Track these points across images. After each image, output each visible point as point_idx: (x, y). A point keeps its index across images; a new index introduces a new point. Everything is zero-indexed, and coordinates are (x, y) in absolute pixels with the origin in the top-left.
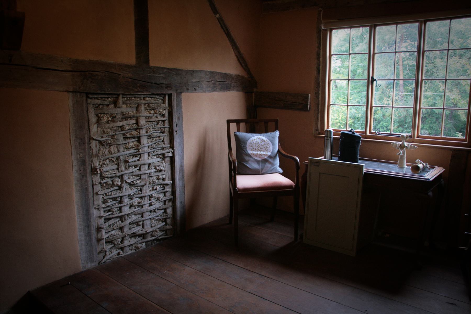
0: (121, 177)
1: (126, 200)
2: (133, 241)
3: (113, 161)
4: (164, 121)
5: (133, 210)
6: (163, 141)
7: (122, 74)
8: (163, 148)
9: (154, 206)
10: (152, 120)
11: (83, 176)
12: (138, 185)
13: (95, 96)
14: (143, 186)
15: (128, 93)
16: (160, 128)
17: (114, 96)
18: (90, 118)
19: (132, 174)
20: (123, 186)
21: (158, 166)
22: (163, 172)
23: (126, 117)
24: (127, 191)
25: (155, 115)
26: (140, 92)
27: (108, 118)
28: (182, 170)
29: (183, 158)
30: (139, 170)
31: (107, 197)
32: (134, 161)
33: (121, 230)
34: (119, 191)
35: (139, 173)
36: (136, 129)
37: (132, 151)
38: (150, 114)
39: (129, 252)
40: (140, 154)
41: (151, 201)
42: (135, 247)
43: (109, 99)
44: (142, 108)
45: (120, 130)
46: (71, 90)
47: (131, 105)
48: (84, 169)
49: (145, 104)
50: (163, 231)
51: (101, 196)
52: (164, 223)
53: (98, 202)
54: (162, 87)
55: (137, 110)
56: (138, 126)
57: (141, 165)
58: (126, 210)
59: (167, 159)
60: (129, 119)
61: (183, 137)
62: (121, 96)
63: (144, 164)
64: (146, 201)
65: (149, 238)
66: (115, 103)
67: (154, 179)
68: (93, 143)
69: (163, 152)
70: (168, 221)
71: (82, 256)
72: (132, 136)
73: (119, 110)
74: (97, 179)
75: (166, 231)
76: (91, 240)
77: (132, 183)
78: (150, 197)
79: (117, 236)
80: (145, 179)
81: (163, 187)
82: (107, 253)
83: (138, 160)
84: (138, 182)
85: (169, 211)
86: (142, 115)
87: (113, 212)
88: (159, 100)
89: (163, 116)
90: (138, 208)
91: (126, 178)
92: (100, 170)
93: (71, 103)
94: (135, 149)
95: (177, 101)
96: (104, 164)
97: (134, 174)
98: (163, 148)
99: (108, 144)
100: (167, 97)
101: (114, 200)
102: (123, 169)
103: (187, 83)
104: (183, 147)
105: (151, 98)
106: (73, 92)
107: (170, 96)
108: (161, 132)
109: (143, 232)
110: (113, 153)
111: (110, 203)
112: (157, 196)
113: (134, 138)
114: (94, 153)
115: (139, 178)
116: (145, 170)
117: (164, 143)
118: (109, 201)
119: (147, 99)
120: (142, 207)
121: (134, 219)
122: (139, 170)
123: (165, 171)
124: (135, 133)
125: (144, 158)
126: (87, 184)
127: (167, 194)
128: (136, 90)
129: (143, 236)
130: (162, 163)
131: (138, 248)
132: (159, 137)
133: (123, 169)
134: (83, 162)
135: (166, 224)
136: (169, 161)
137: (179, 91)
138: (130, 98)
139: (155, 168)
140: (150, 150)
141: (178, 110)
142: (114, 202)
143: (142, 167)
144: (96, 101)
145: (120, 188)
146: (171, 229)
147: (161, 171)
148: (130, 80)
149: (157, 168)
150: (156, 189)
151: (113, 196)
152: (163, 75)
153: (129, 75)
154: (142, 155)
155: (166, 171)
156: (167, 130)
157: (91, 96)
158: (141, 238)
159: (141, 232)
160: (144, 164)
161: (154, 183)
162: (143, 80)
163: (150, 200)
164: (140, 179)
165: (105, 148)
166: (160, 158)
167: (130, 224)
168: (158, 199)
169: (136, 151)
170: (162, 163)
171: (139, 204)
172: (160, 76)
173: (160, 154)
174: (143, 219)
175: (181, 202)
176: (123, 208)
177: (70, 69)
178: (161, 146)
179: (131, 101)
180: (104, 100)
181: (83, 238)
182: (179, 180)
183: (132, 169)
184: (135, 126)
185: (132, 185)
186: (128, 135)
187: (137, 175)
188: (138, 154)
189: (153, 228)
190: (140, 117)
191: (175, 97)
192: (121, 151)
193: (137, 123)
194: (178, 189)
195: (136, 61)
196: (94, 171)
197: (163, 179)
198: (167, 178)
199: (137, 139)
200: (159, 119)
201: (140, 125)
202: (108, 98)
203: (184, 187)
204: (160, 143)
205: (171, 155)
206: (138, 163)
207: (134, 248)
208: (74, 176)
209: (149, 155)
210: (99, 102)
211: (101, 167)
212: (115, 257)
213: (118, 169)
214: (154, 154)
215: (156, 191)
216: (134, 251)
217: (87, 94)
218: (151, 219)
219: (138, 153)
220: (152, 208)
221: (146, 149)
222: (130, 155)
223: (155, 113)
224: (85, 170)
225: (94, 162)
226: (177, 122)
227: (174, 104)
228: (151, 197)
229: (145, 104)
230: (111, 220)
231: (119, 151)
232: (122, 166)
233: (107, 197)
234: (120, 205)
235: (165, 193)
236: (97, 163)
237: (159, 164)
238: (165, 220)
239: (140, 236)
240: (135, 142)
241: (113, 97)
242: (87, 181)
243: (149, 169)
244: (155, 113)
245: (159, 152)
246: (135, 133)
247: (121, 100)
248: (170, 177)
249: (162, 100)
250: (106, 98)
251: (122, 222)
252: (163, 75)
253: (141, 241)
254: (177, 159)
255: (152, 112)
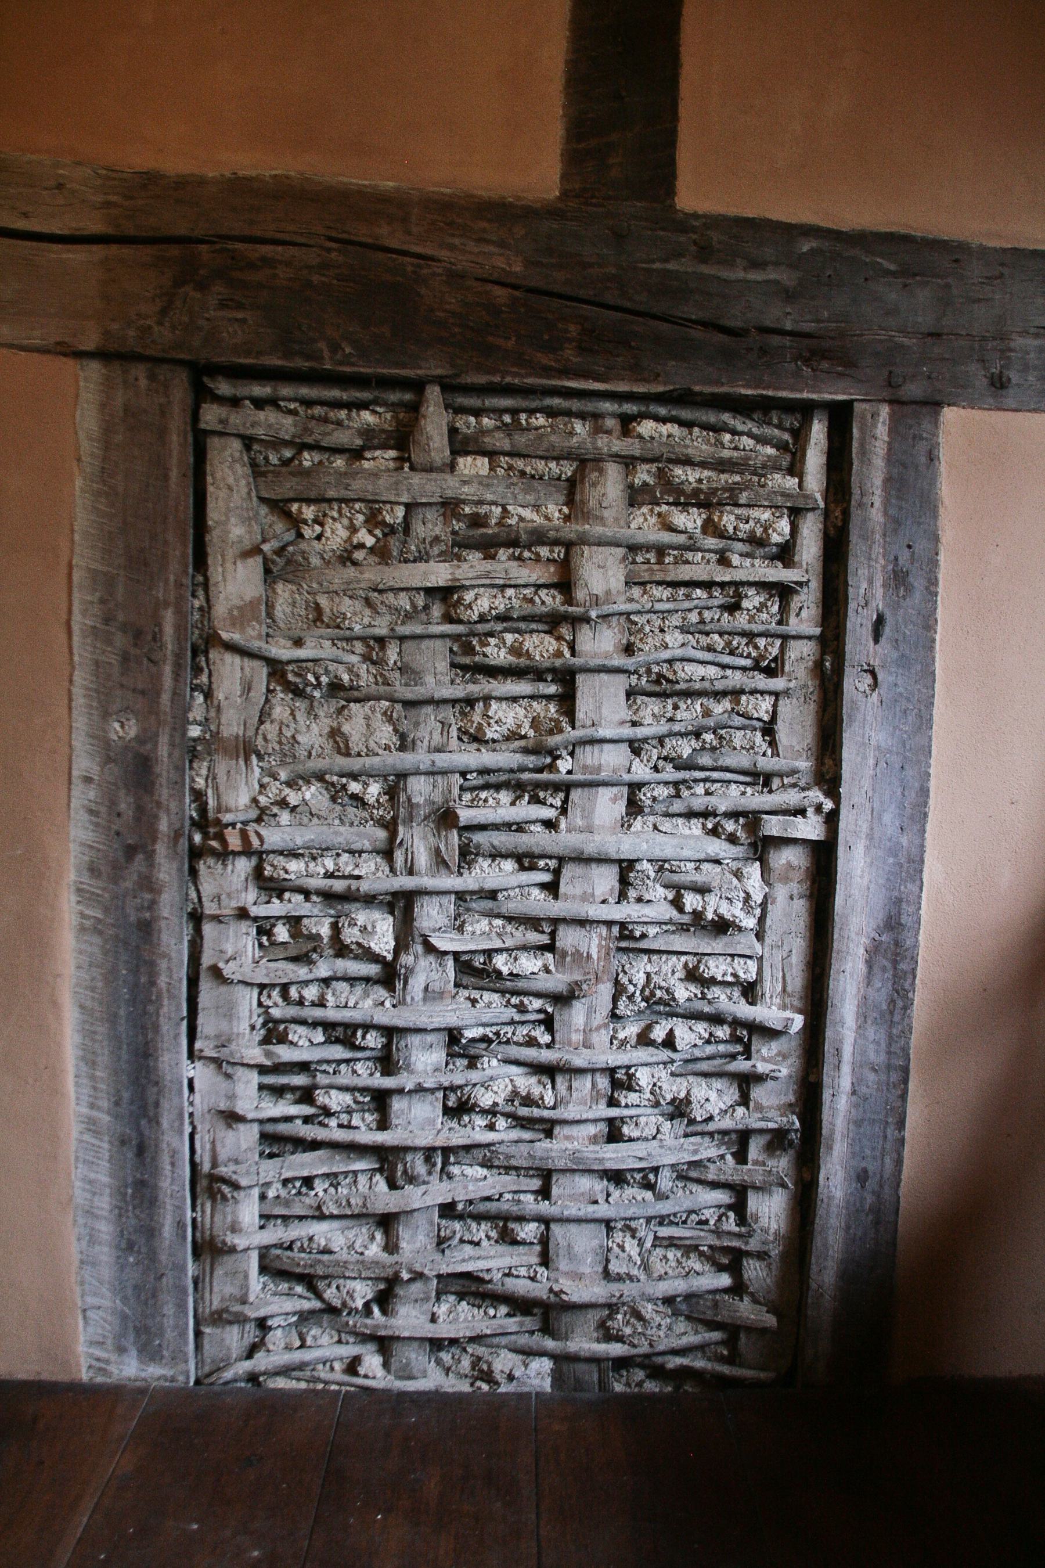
0: (402, 905)
1: (425, 1060)
2: (461, 1318)
3: (358, 800)
4: (784, 592)
5: (474, 1131)
6: (769, 730)
7: (443, 254)
8: (763, 779)
9: (639, 1149)
10: (685, 573)
11: (131, 851)
12: (521, 984)
13: (259, 390)
14: (564, 999)
15: (481, 379)
16: (750, 636)
17: (394, 397)
18: (214, 514)
19: (488, 904)
20: (410, 971)
21: (703, 890)
22: (746, 943)
23: (484, 538)
24: (434, 998)
25: (711, 542)
26: (585, 375)
27: (353, 529)
28: (893, 949)
29: (910, 867)
30: (552, 888)
31: (292, 1011)
32: (519, 827)
33: (387, 1233)
34: (381, 992)
35: (539, 903)
36: (553, 622)
37: (505, 758)
38: (672, 529)
39: (431, 1378)
40: (565, 788)
41: (614, 1112)
42: (477, 1361)
43: (367, 416)
44: (610, 487)
45: (437, 611)
46: (89, 346)
47: (520, 463)
48: (140, 809)
49: (629, 463)
50: (712, 1325)
51: (248, 998)
52: (725, 1280)
53: (224, 1026)
54: (763, 351)
55: (570, 502)
56: (569, 600)
57: (561, 860)
58: (418, 1122)
59: (789, 859)
60: (503, 554)
61: (925, 722)
62: (433, 393)
63: (584, 859)
64: (582, 1102)
65: (583, 1342)
66: (402, 440)
67: (669, 973)
68: (229, 674)
69: (755, 799)
70: (754, 1271)
71: (91, 1300)
72: (523, 661)
73: (425, 487)
74: (229, 882)
75: (733, 1331)
76: (151, 1232)
77: (479, 961)
78: (616, 1084)
79: (343, 1255)
80: (581, 958)
81: (735, 1039)
82: (276, 1338)
83: (550, 825)
84: (529, 964)
85: (770, 1210)
86: (598, 530)
87: (327, 1112)
88: (747, 440)
89: (785, 554)
90: (515, 1134)
91: (431, 916)
92: (244, 835)
93: (88, 420)
94: (526, 751)
95: (890, 458)
96: (283, 803)
97: (512, 907)
98: (763, 779)
99: (336, 688)
100: (818, 431)
101: (338, 1041)
102: (423, 859)
103: (1003, 337)
104: (924, 792)
105: (682, 423)
106: (102, 355)
107: (840, 418)
108: (756, 667)
109: (539, 1290)
110: (356, 743)
111: (304, 1045)
112: (673, 1088)
113: (538, 674)
114: (232, 725)
115: (545, 939)
116: (587, 898)
117: (773, 744)
118: (298, 1034)
119: (647, 428)
120: (549, 1134)
121: (475, 1191)
122: (552, 888)
123: (760, 936)
124: (541, 647)
125: (588, 814)
126: (153, 904)
127: (758, 1093)
128: (546, 360)
129: (548, 1313)
130: (738, 874)
131: (487, 1376)
132: (736, 693)
133: (423, 859)
134: (136, 771)
135: (738, 1289)
136: (797, 876)
137: (913, 390)
138: (514, 412)
139: (677, 903)
140: (641, 771)
141: (894, 524)
142: (338, 1052)
143: (569, 872)
144: (268, 416)
145: (390, 976)
146: (763, 1331)
147: (722, 927)
148: (500, 293)
149: (691, 901)
150: (669, 1042)
151: (331, 1014)
152: (785, 276)
153: (500, 263)
154: (575, 795)
155: (770, 938)
156: (801, 655)
157: (224, 388)
158: (529, 1323)
159: (521, 1287)
160: (584, 859)
161: (659, 1004)
162: (609, 298)
163: (612, 1103)
164: (550, 948)
165: (310, 711)
166: (732, 839)
167: (448, 1210)
168: (679, 1110)
169: (531, 761)
170: (738, 874)
171: (524, 1111)
172: (754, 276)
173: (734, 815)
174: (544, 1207)
175: (862, 1177)
176: (397, 1104)
177: (95, 226)
178: (743, 761)
179: (521, 440)
180: (325, 420)
181: (104, 1203)
182: (863, 1017)
183: (500, 874)
184: (550, 601)
185: (474, 972)
186: (497, 654)
187: (533, 922)
188: (541, 779)
189: (615, 1288)
190: (584, 540)
191: (875, 430)
192: (422, 747)
193: (565, 585)
194: (845, 1082)
195: (564, 177)
196: (207, 838)
197: (750, 991)
198: (770, 986)
199: (552, 689)
200: (739, 575)
201: (580, 595)
202: (363, 405)
203: (898, 1073)
204: (738, 738)
205: (810, 828)
206: (538, 838)
207: (466, 1363)
208: (74, 838)
209: (634, 808)
210: (286, 426)
211: (259, 820)
212: (323, 1373)
213: (388, 854)
214: (678, 806)
215: (665, 1054)
216: (465, 1387)
217: (201, 379)
218: (608, 1224)
219: (545, 776)
220: (615, 1156)
221: (612, 759)
222: (491, 781)
223: (710, 527)
224: (144, 819)
225: (222, 778)
226: (879, 601)
227: (872, 475)
228: (620, 1081)
229: (629, 463)
230: (308, 1157)
231: (405, 744)
232: (419, 842)
233: (292, 1011)
234: (380, 1081)
235: (746, 1082)
236: (238, 793)
237: (710, 873)
238: (732, 1261)
239: (520, 1305)
240: (537, 706)
241: (392, 406)
242: (148, 884)
243: (622, 896)
244: (710, 527)
245: (734, 796)
246: (541, 647)
247: (435, 424)
248: (797, 980)
249: (782, 447)
250: (349, 406)
251: (392, 1185)
252: (785, 276)
253: (523, 1340)
254: (857, 873)
255: (690, 520)
